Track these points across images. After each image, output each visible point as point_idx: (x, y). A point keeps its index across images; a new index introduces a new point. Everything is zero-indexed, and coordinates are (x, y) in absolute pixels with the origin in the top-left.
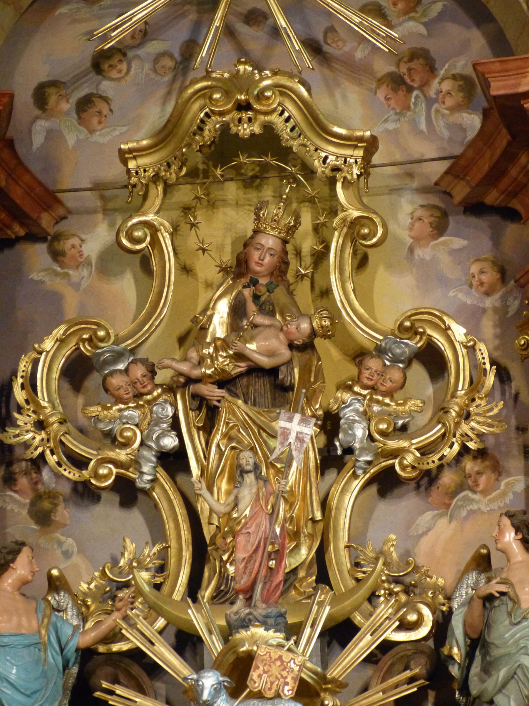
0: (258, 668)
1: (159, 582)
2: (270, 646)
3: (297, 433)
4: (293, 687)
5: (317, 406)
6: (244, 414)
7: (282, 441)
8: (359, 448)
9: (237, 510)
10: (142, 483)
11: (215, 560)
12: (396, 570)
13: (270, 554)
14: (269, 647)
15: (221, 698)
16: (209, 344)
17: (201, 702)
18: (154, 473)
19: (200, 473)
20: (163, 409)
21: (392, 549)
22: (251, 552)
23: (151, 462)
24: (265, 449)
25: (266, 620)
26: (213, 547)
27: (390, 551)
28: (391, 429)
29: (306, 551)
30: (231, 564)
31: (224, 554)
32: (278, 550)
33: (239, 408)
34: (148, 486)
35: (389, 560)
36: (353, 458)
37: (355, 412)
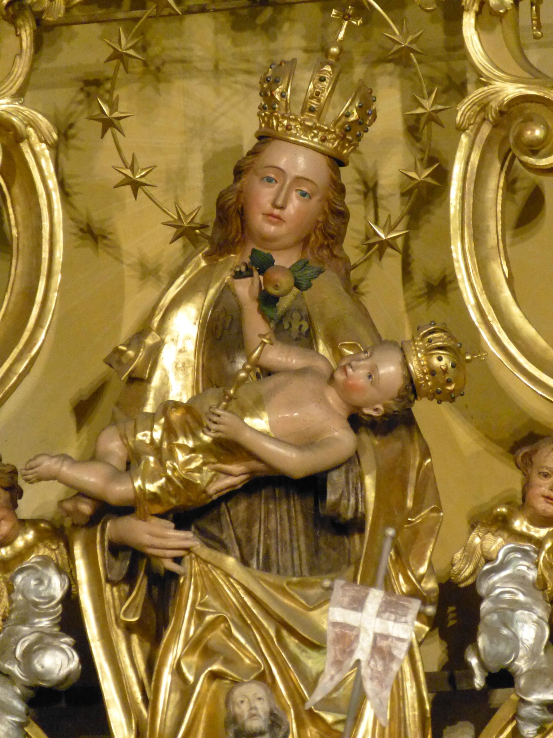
3: (376, 636)
5: (423, 570)
6: (241, 592)
7: (339, 657)
8: (528, 671)
16: (153, 418)
20: (40, 582)
23: (11, 711)
24: (295, 676)
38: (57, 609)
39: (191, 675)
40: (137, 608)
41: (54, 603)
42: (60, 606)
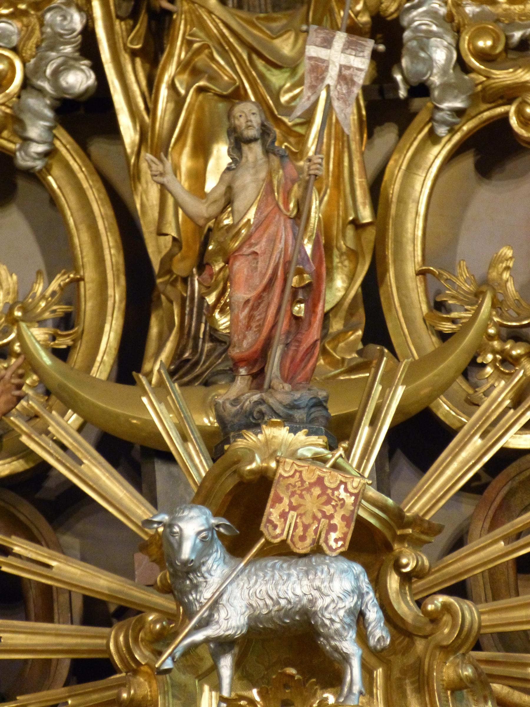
0: (279, 500)
1: (64, 347)
2: (300, 459)
3: (341, 66)
4: (345, 535)
5: (359, 7)
6: (221, 26)
7: (314, 83)
8: (441, 85)
9: (232, 212)
10: (27, 158)
11: (171, 302)
12: (514, 315)
13: (295, 291)
14: (299, 463)
15: (214, 555)
17: (179, 564)
18: (49, 140)
19: (137, 138)
20: (65, 18)
21: (506, 275)
22: (260, 289)
23: (43, 118)
24: (263, 90)
25: (291, 412)
26: (167, 277)
27: (501, 279)
28: (500, 48)
29: (343, 282)
30: (222, 312)
31: (209, 294)
32: (310, 284)
33: (210, 13)
34: (39, 164)
35: (500, 297)
36: (429, 105)
37: (431, 17)
38: (77, 39)
39: (183, 89)
40: (140, 37)
41: (75, 34)
42: (80, 36)
